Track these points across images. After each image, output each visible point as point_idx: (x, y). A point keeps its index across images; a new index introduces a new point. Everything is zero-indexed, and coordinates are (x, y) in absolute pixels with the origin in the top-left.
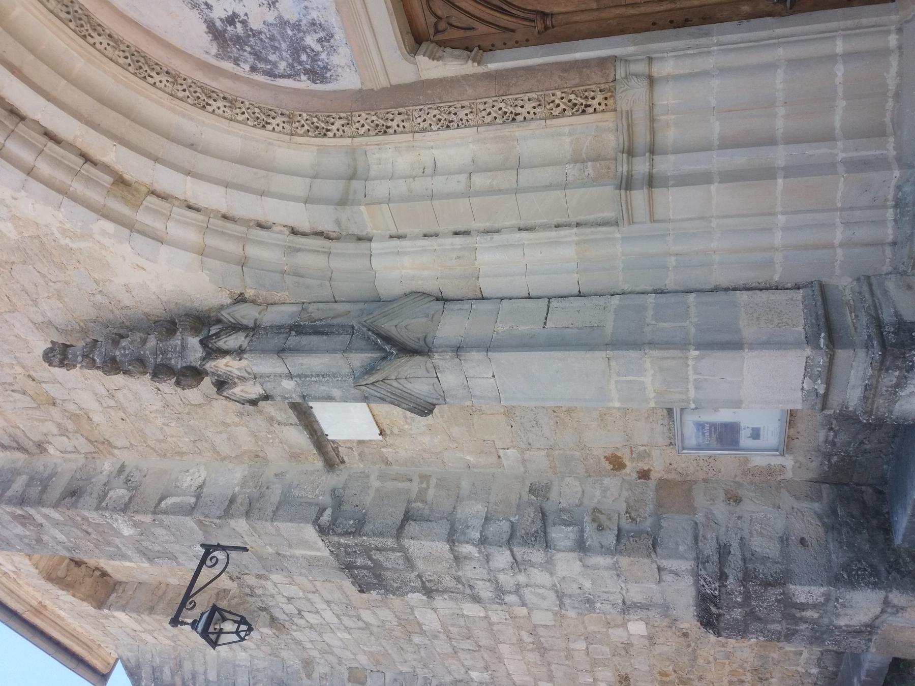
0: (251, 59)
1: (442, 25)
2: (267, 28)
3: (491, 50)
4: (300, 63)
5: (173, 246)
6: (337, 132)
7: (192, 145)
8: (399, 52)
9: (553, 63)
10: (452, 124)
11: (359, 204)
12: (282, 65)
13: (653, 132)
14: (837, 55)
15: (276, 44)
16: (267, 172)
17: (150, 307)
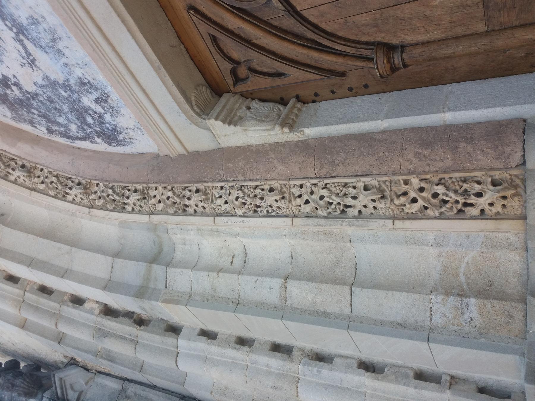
3: (314, 101)
8: (183, 117)
9: (406, 130)
15: (58, 107)
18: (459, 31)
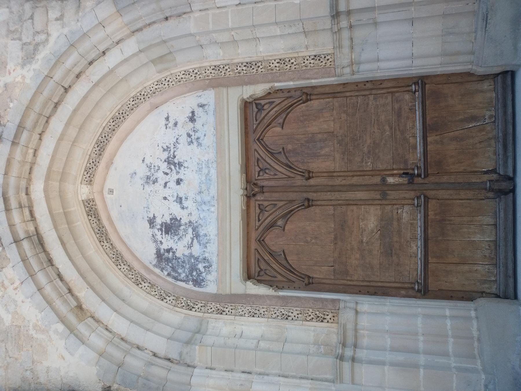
0: (169, 269)
1: (262, 273)
2: (183, 257)
3: (281, 289)
4: (192, 276)
5: (88, 347)
6: (197, 309)
7: (124, 300)
8: (239, 278)
10: (256, 315)
11: (196, 345)
12: (183, 275)
13: (356, 337)
14: (447, 316)
15: (184, 265)
16: (154, 321)
17: (53, 385)
18: (327, 277)
